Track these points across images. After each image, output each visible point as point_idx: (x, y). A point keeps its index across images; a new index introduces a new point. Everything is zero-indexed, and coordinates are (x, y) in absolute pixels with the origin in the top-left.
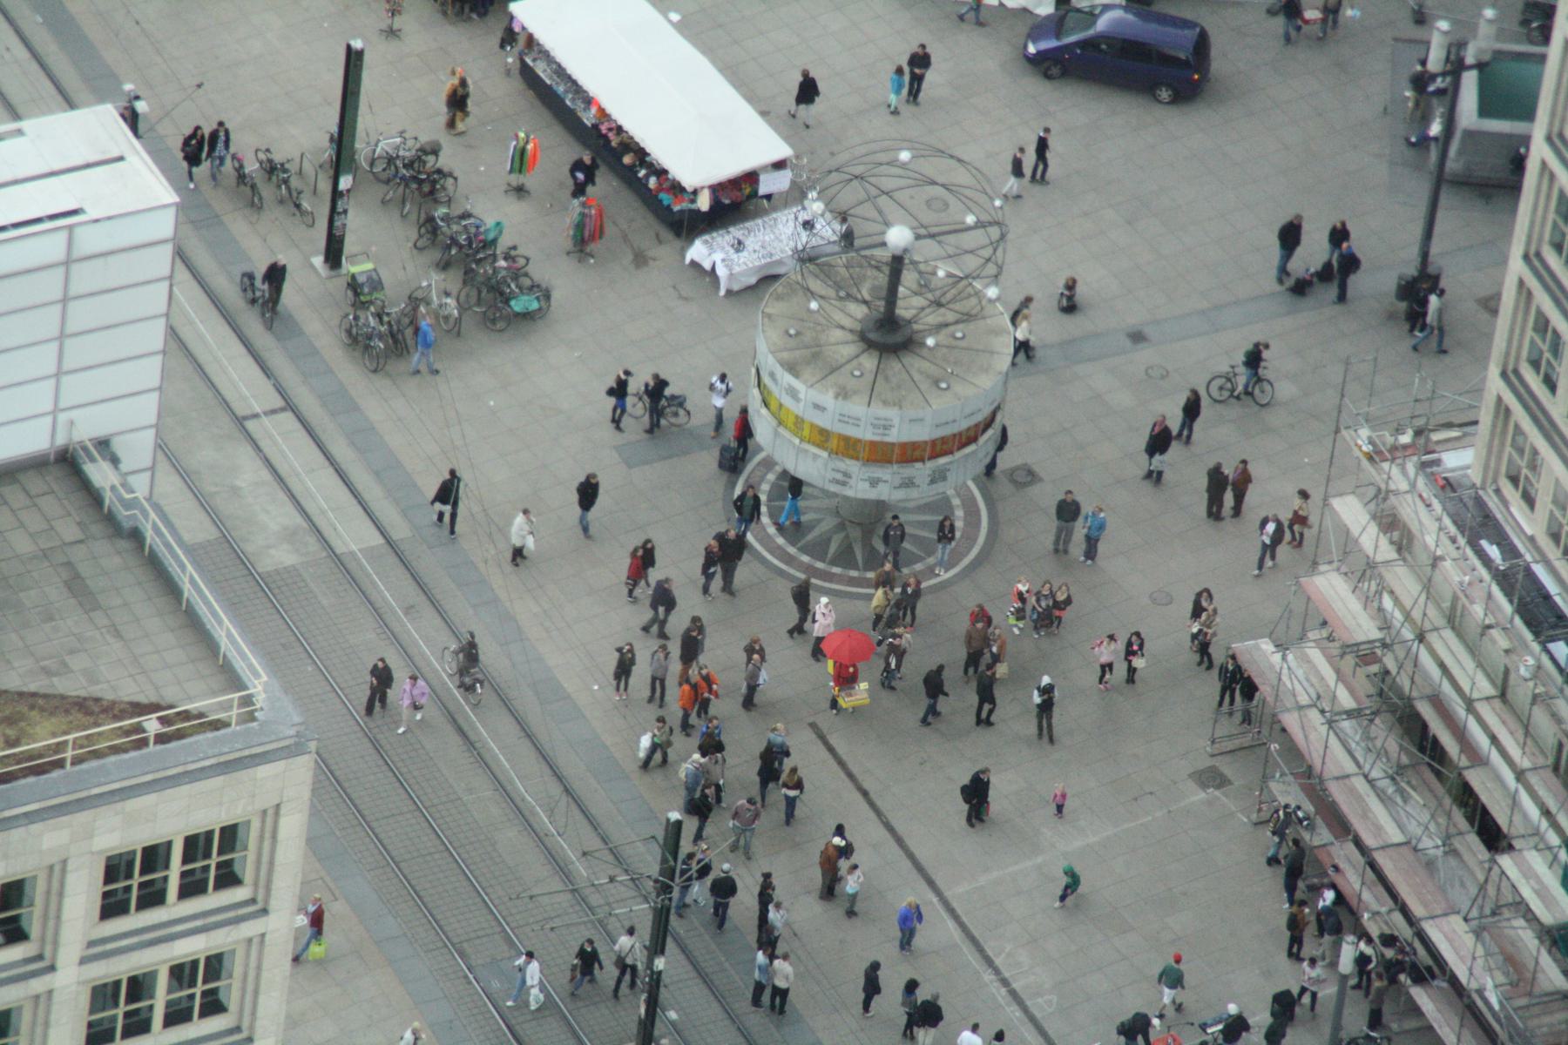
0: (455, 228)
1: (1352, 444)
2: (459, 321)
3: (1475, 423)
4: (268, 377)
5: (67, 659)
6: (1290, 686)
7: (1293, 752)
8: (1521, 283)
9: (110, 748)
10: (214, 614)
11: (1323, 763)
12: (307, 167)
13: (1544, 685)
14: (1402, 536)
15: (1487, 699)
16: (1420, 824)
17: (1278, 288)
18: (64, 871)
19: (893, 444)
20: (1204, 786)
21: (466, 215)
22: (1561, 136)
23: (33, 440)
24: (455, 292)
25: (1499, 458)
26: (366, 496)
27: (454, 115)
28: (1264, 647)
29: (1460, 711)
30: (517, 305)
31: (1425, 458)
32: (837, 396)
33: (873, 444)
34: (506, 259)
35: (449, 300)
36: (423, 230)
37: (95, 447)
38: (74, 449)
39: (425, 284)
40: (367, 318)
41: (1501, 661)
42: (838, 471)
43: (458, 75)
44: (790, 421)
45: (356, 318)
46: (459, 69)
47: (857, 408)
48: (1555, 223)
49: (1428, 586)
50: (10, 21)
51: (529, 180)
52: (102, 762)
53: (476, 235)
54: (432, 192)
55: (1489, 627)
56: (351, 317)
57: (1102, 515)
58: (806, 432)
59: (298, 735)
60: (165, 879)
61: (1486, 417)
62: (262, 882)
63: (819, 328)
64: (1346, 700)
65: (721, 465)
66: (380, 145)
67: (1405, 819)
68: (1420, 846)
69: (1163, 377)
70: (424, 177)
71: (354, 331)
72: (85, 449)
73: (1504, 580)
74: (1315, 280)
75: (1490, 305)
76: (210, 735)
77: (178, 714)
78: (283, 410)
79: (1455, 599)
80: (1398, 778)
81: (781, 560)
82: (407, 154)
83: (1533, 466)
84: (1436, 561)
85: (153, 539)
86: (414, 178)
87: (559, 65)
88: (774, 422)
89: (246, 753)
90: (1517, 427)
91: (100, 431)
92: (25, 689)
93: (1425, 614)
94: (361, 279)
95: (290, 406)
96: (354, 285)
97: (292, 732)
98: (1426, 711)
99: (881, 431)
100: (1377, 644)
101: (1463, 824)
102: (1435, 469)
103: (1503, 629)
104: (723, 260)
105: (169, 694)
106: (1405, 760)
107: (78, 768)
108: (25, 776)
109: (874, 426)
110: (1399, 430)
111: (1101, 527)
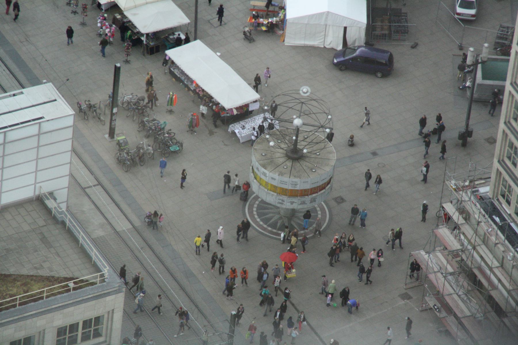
0: (151, 124)
1: (449, 186)
2: (153, 154)
3: (490, 178)
4: (92, 174)
5: (42, 264)
6: (431, 265)
7: (432, 286)
8: (504, 131)
9: (58, 292)
10: (90, 248)
11: (443, 290)
12: (102, 106)
13: (516, 262)
14: (466, 216)
15: (497, 267)
16: (476, 309)
17: (420, 137)
18: (113, 312)
19: (298, 190)
20: (403, 299)
21: (154, 120)
22: (515, 83)
23: (28, 193)
24: (151, 145)
25: (498, 189)
26: (126, 212)
27: (149, 88)
28: (422, 253)
29: (488, 272)
30: (172, 149)
31: (473, 190)
32: (279, 175)
33: (291, 190)
34: (167, 134)
35: (150, 148)
36: (140, 125)
37: (48, 195)
38: (42, 196)
39: (142, 143)
40: (123, 154)
41: (500, 255)
42: (280, 199)
43: (150, 75)
44: (264, 184)
45: (120, 154)
46: (150, 73)
47: (286, 179)
48: (514, 111)
49: (476, 232)
50: (3, 62)
51: (173, 108)
52: (56, 297)
53: (158, 126)
54: (143, 113)
55: (497, 244)
56: (119, 154)
57: (366, 211)
58: (269, 187)
59: (119, 286)
60: (77, 335)
61: (493, 176)
62: (108, 335)
63: (272, 153)
64: (450, 269)
65: (241, 199)
66: (125, 98)
67: (470, 308)
68: (476, 316)
69: (383, 167)
70: (140, 108)
71: (120, 158)
72: (45, 196)
73: (502, 228)
74: (431, 134)
75: (492, 141)
76: (90, 287)
77: (80, 281)
78: (98, 185)
79: (485, 234)
80: (468, 294)
81: (262, 230)
82: (134, 101)
83: (509, 192)
84: (479, 223)
85: (69, 224)
86: (137, 108)
87: (182, 70)
88: (259, 184)
89: (103, 292)
90: (504, 178)
91: (50, 190)
92: (29, 274)
93: (475, 240)
94: (121, 142)
95: (100, 184)
96: (119, 144)
97: (117, 285)
98: (476, 272)
99: (293, 186)
100: (460, 251)
101: (490, 309)
102: (477, 193)
103: (502, 244)
104: (238, 132)
105: (76, 274)
106: (470, 288)
107: (48, 299)
108: (31, 302)
109: (292, 185)
110: (465, 181)
111: (366, 215)
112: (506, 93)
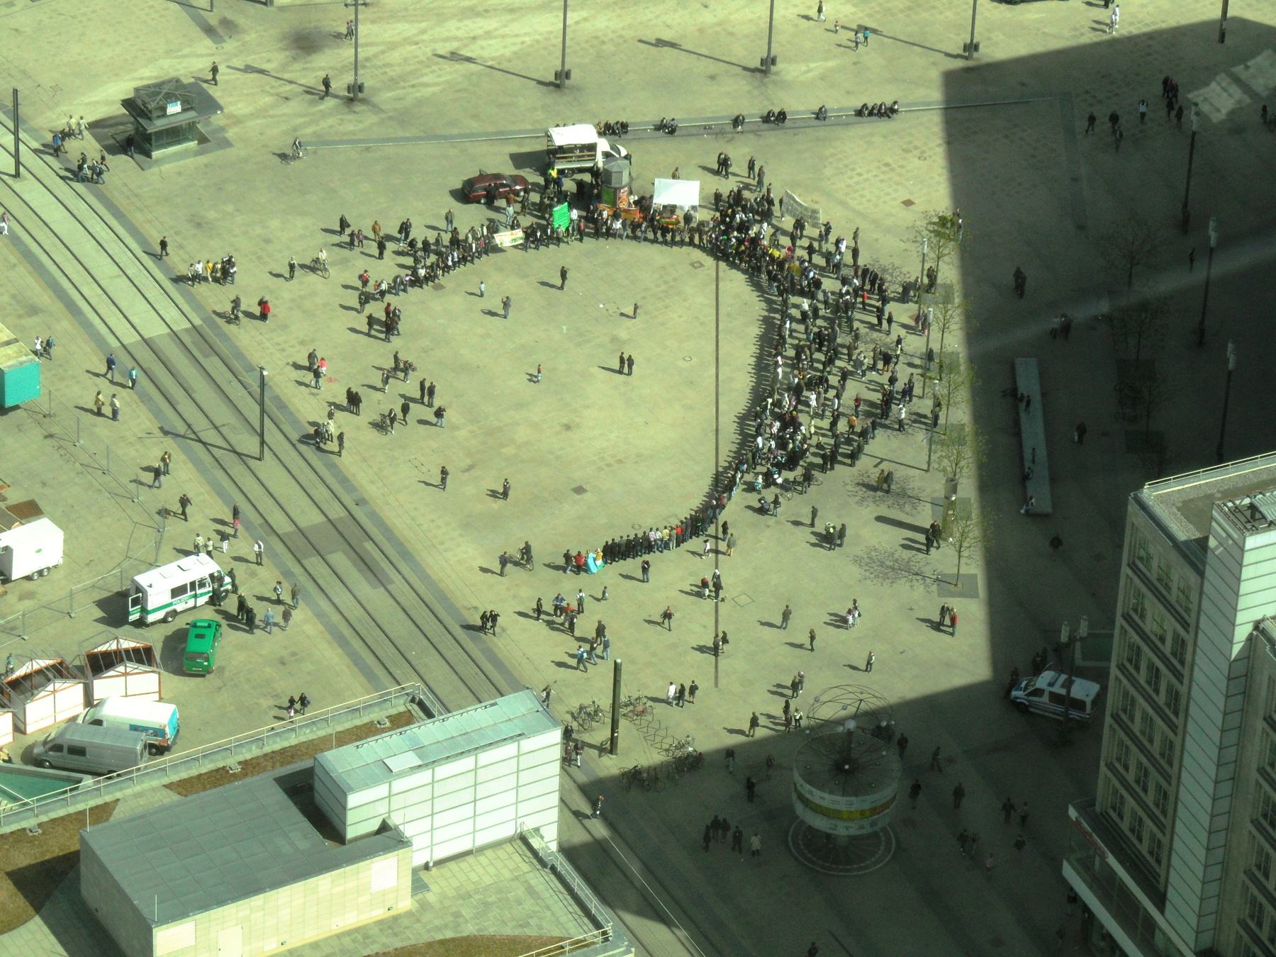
112: (1112, 677)
